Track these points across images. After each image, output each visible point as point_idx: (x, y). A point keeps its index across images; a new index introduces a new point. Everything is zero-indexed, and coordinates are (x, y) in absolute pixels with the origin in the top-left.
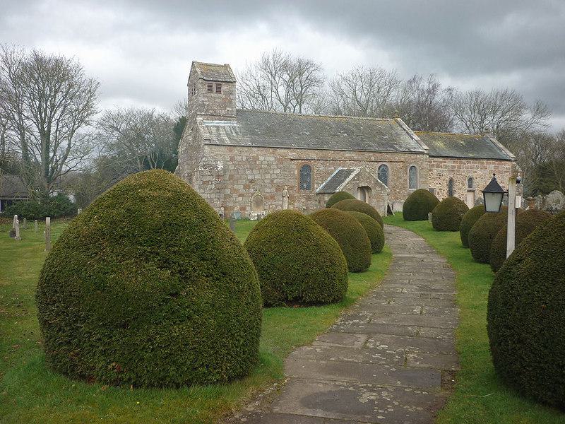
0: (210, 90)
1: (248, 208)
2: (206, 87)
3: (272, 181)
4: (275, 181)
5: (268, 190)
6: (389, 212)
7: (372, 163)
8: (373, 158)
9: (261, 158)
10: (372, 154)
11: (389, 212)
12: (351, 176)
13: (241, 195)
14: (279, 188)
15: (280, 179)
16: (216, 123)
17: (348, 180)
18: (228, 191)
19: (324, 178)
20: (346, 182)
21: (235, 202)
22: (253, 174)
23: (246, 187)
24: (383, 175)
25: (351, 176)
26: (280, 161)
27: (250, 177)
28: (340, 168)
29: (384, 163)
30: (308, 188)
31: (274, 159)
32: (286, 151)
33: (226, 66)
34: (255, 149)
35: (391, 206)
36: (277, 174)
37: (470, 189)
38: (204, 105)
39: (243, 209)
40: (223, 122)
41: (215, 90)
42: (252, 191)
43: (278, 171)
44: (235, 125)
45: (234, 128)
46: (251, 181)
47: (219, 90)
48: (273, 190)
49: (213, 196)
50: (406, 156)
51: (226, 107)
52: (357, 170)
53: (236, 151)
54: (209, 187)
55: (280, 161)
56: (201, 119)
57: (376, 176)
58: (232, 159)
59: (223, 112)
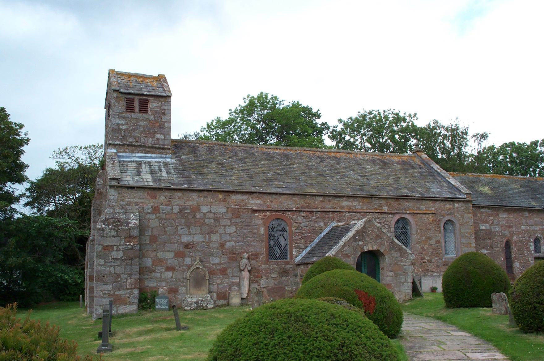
0: (130, 108)
1: (182, 290)
2: (123, 103)
3: (222, 245)
4: (228, 245)
5: (217, 261)
6: (416, 291)
7: (385, 216)
8: (385, 209)
9: (204, 209)
10: (383, 202)
11: (416, 291)
12: (350, 234)
13: (169, 269)
14: (234, 257)
15: (236, 242)
16: (137, 156)
17: (344, 239)
18: (149, 262)
19: (308, 240)
20: (341, 243)
21: (160, 280)
22: (190, 233)
23: (179, 255)
24: (402, 231)
25: (350, 234)
26: (236, 213)
27: (186, 239)
28: (334, 224)
29: (404, 216)
30: (283, 255)
31: (224, 210)
32: (244, 197)
33: (161, 79)
34: (194, 195)
35: (417, 283)
36: (230, 234)
37: (537, 255)
38: (120, 130)
39: (173, 291)
40: (149, 155)
41: (137, 109)
42: (188, 261)
43: (232, 229)
44: (168, 160)
45: (166, 164)
46: (187, 246)
47: (144, 108)
48: (225, 259)
49: (119, 270)
50: (438, 204)
51: (155, 133)
52: (359, 224)
53: (162, 197)
54: (114, 255)
55: (236, 213)
56: (114, 150)
57: (391, 235)
58: (155, 210)
59: (149, 142)
